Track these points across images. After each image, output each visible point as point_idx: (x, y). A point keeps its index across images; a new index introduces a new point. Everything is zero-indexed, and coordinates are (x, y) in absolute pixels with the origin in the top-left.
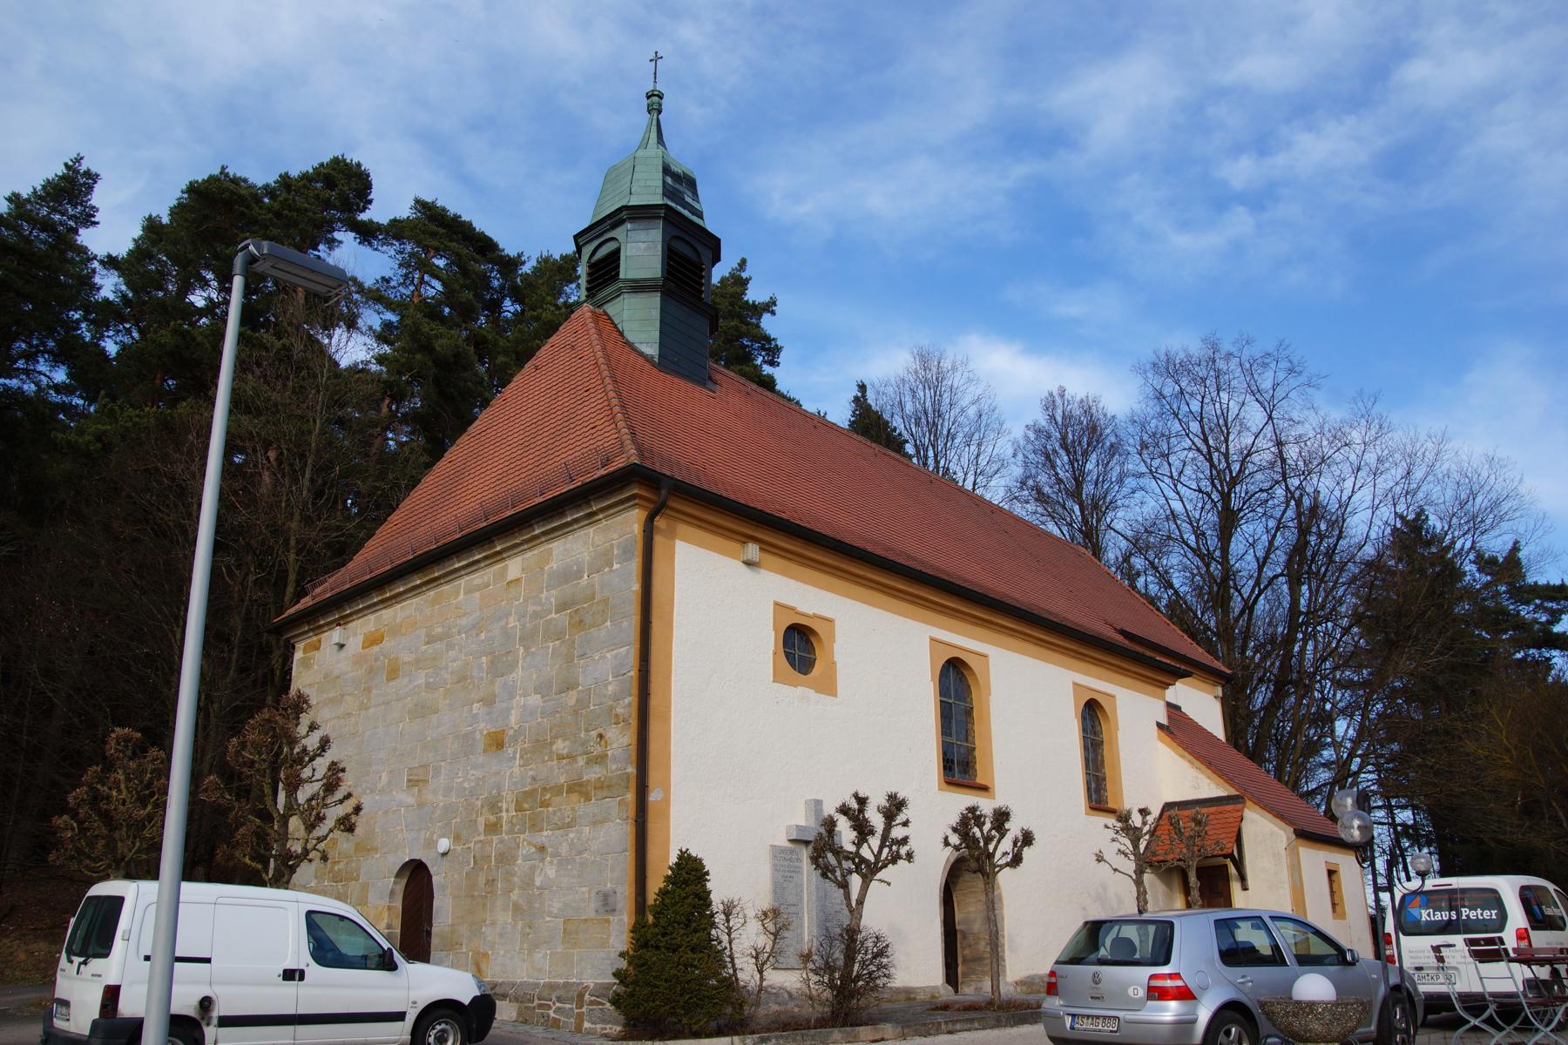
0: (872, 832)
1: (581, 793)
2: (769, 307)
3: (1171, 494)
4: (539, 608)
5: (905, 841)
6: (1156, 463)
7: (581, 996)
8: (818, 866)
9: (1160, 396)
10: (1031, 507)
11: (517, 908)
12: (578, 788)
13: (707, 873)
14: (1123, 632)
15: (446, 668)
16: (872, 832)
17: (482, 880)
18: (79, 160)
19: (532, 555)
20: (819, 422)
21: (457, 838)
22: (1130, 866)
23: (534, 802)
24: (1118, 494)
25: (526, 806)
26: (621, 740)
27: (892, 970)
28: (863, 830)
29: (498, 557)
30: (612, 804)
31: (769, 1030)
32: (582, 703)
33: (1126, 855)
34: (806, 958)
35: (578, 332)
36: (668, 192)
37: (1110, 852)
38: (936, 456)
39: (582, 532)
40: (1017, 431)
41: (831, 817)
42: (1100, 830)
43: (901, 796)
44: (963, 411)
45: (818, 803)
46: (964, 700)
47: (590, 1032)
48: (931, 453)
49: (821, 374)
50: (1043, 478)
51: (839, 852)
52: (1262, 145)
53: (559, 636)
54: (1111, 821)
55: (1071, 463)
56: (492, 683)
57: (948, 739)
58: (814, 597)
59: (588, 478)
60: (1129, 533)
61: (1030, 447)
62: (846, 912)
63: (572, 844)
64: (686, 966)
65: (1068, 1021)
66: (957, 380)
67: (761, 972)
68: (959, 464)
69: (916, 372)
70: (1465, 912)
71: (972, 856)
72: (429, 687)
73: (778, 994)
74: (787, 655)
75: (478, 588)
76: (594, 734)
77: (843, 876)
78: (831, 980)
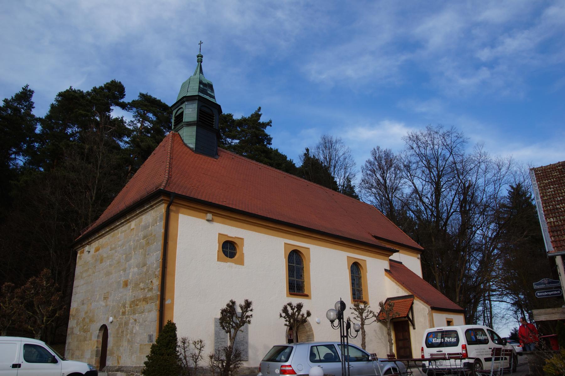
2: (269, 124)
11: (129, 341)
12: (145, 299)
14: (376, 237)
17: (120, 332)
18: (27, 86)
21: (115, 317)
23: (134, 303)
26: (157, 282)
29: (128, 221)
30: (153, 304)
32: (147, 271)
36: (200, 90)
39: (150, 212)
43: (250, 300)
46: (300, 265)
52: (492, 44)
58: (233, 231)
66: (338, 146)
70: (446, 339)
72: (111, 265)
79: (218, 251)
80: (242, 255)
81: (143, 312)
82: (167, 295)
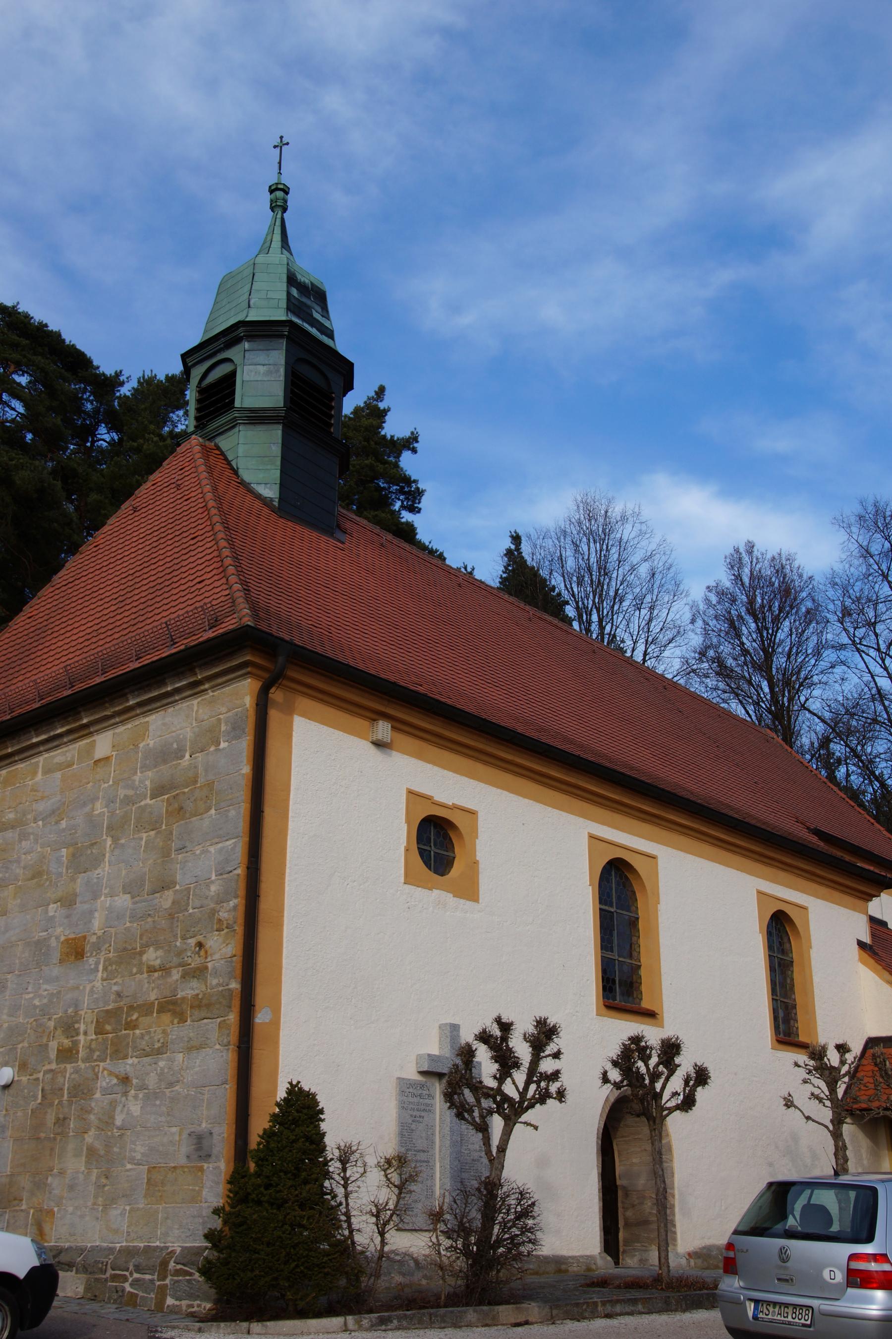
0: (517, 1065)
1: (174, 1013)
2: (410, 443)
3: (878, 670)
4: (130, 792)
5: (555, 1076)
6: (860, 633)
7: (164, 1264)
8: (452, 1105)
9: (866, 553)
10: (710, 682)
11: (92, 1152)
12: (171, 1007)
13: (321, 1111)
14: (817, 833)
15: (18, 861)
16: (517, 1065)
17: (50, 1118)
19: (124, 730)
20: (465, 579)
21: (23, 1067)
22: (825, 1114)
23: (118, 1024)
24: (815, 668)
25: (108, 1028)
26: (224, 949)
27: (539, 1235)
28: (507, 1063)
29: (84, 731)
30: (211, 1026)
31: (390, 1308)
32: (179, 905)
33: (820, 1100)
34: (436, 1217)
35: (186, 465)
36: (292, 306)
37: (801, 1095)
38: (600, 621)
39: (184, 705)
40: (696, 591)
41: (469, 1046)
42: (787, 1069)
43: (552, 1021)
44: (633, 569)
45: (455, 1028)
47: (174, 1310)
48: (595, 618)
49: (466, 526)
50: (726, 649)
51: (478, 1088)
53: (154, 826)
54: (802, 1058)
55: (759, 631)
56: (73, 880)
57: (609, 955)
58: (452, 785)
59: (192, 641)
60: (827, 715)
61: (712, 612)
62: (485, 1161)
63: (162, 1073)
64: (291, 1225)
65: (750, 1308)
66: (627, 532)
67: (382, 1234)
68: (628, 632)
69: (580, 523)
71: (635, 1096)
73: (404, 1260)
74: (423, 854)
75: (60, 767)
76: (192, 942)
77: (482, 1117)
78: (466, 1245)
79: (407, 850)
80: (474, 865)
81: (159, 1052)
82: (261, 994)
